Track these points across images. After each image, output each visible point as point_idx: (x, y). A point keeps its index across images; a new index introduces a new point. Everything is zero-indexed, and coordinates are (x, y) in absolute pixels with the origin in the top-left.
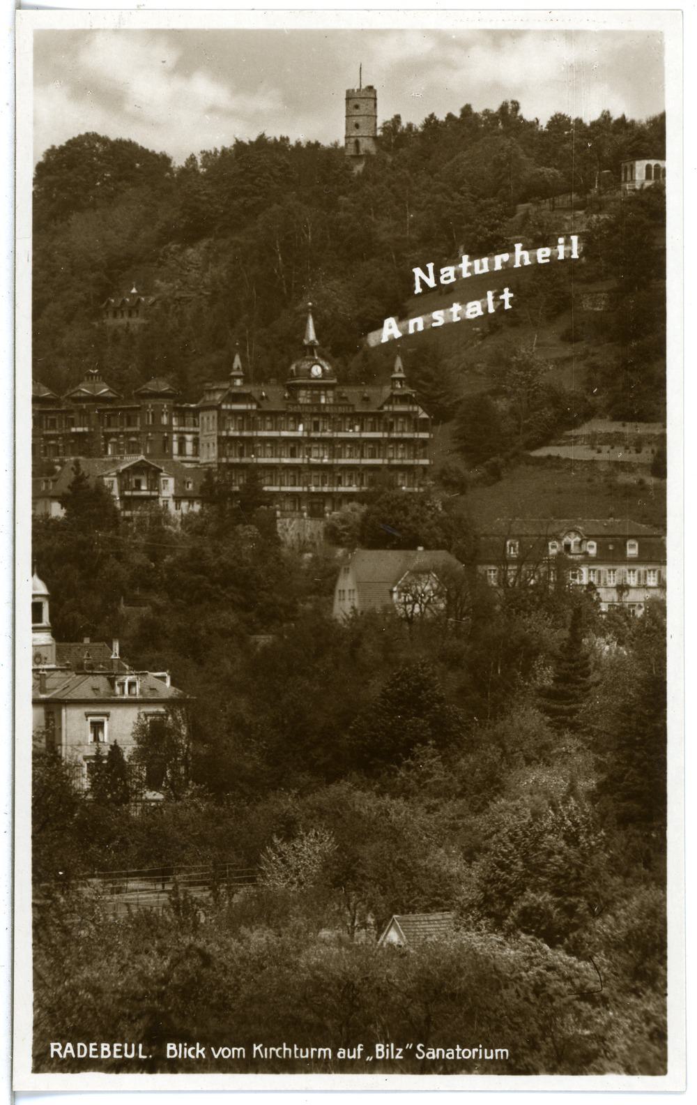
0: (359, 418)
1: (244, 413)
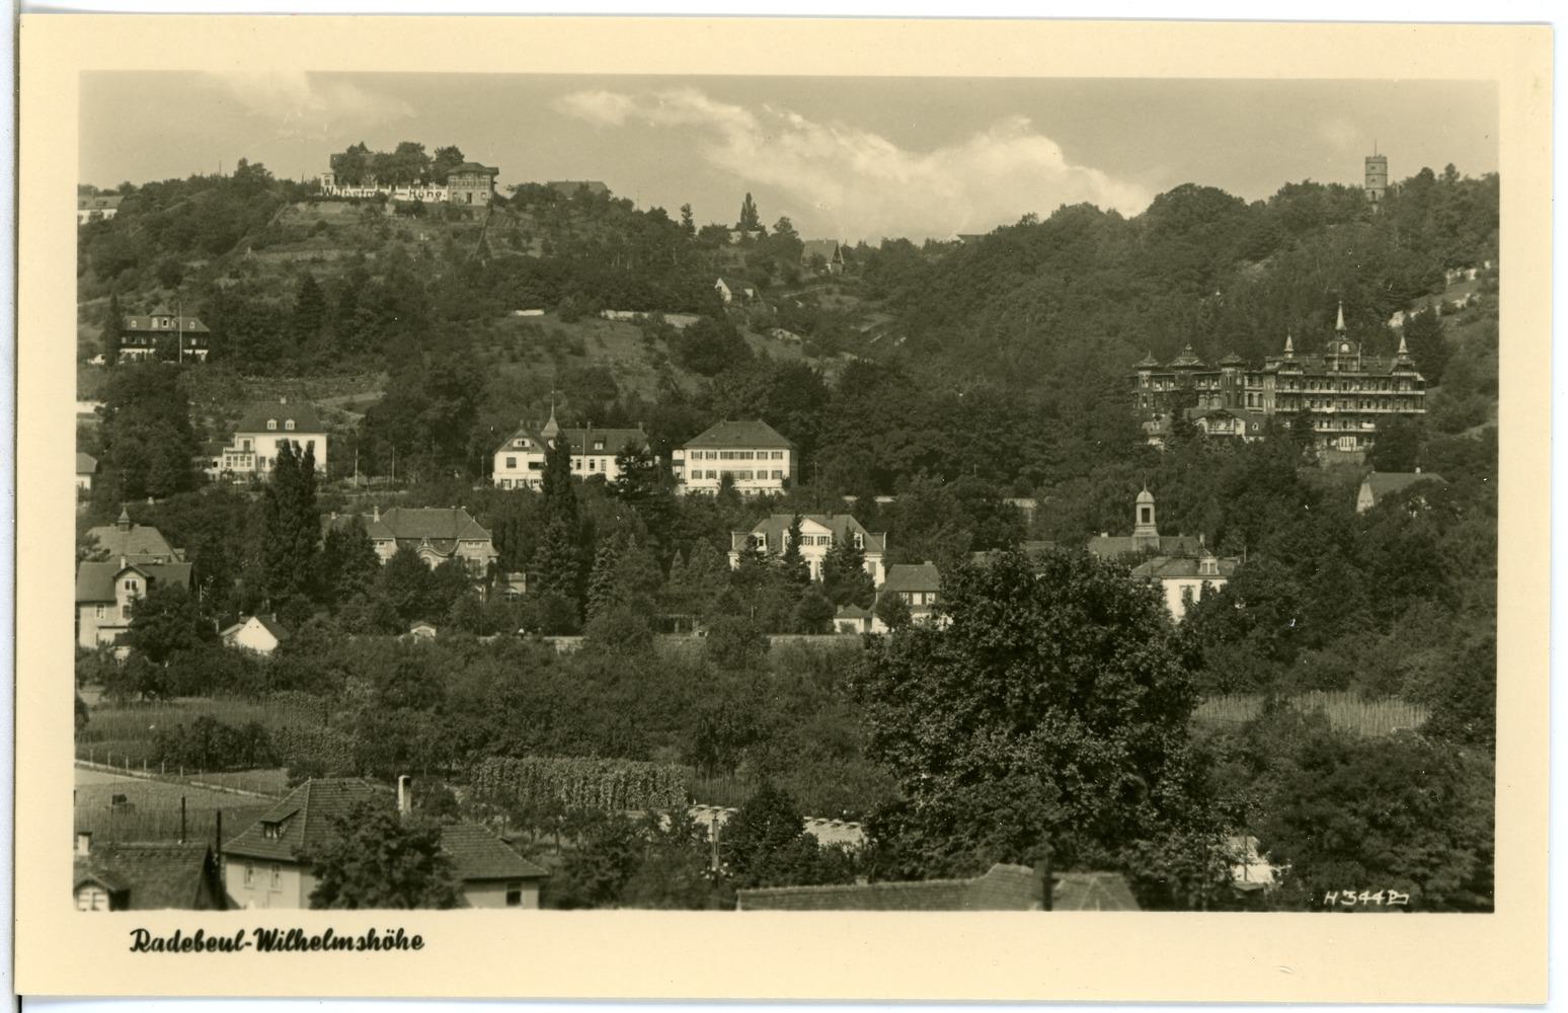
0: (1372, 380)
1: (1295, 377)
